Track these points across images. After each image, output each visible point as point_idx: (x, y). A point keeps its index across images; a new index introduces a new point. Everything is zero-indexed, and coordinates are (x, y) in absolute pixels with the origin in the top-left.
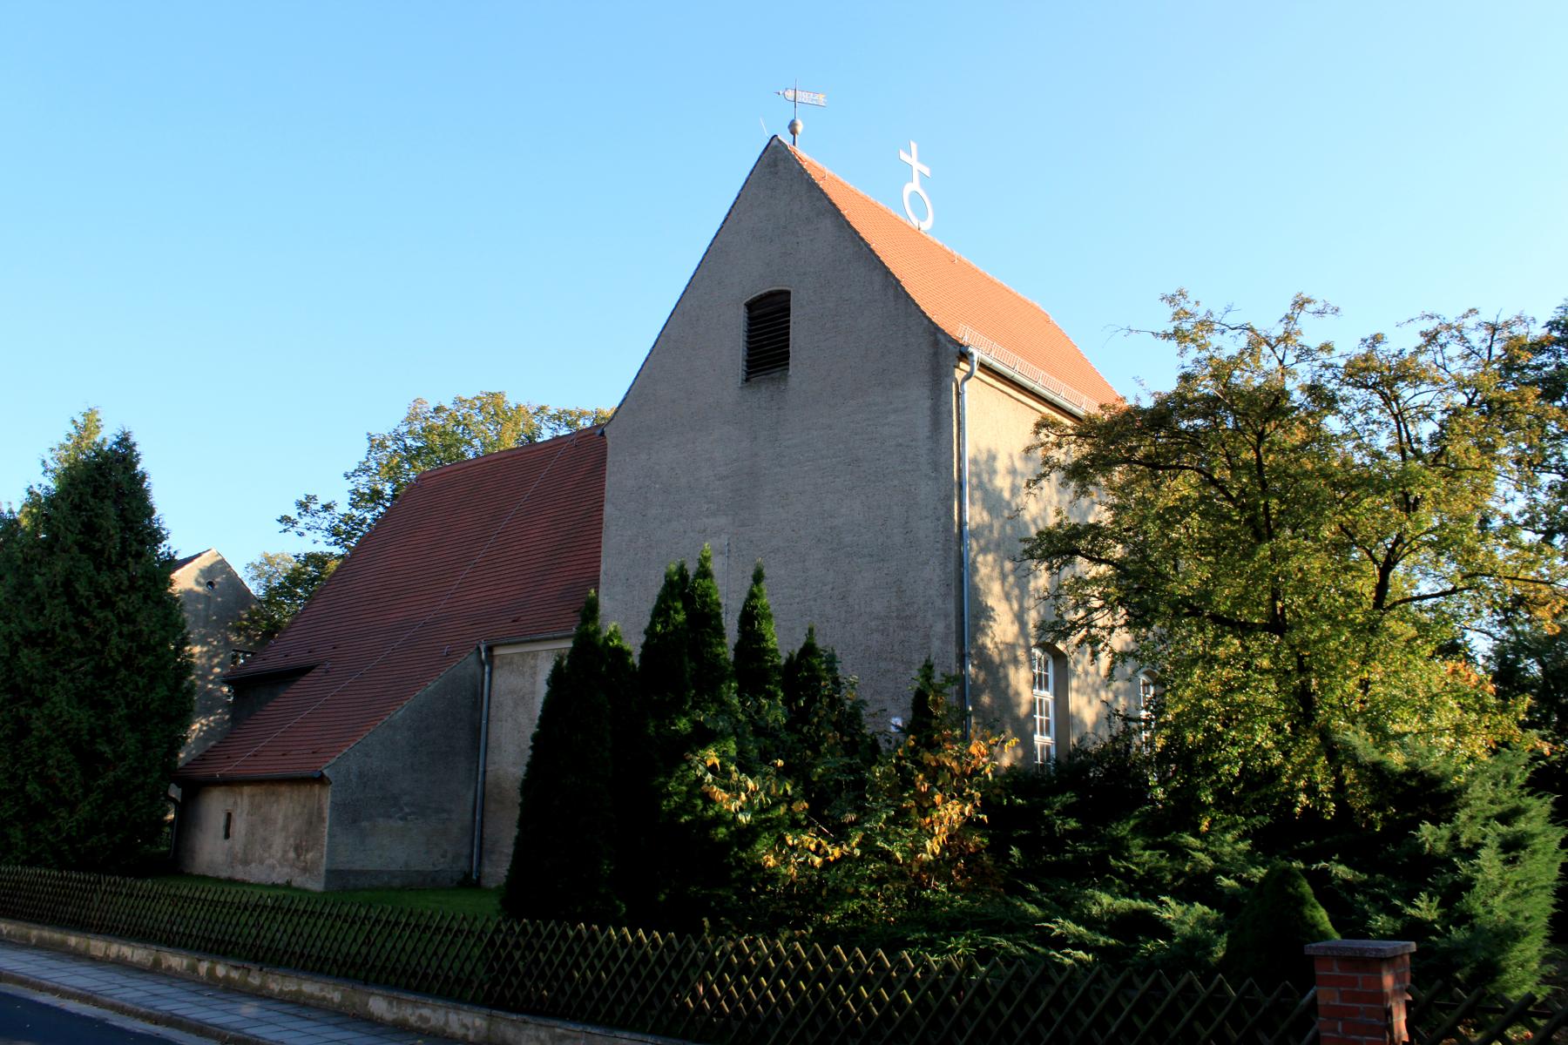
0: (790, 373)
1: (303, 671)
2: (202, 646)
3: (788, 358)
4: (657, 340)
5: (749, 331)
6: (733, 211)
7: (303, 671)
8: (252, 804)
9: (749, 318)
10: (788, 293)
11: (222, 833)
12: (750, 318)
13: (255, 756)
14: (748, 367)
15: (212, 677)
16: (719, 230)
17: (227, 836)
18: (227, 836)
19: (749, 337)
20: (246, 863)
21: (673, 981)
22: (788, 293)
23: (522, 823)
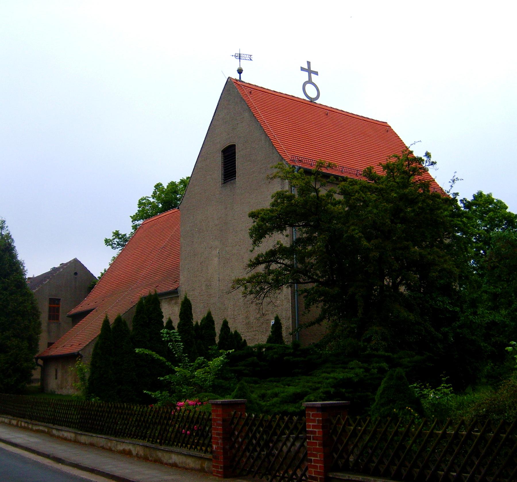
0: (236, 180)
1: (91, 310)
2: (484, 252)
3: (235, 174)
4: (194, 168)
5: (224, 167)
6: (216, 111)
7: (91, 310)
8: (413, 175)
9: (224, 157)
10: (235, 145)
11: (54, 377)
12: (224, 157)
13: (63, 347)
14: (225, 178)
15: (447, 241)
16: (212, 120)
17: (56, 378)
18: (56, 378)
19: (224, 165)
20: (62, 388)
21: (261, 445)
22: (235, 145)
23: (86, 479)
